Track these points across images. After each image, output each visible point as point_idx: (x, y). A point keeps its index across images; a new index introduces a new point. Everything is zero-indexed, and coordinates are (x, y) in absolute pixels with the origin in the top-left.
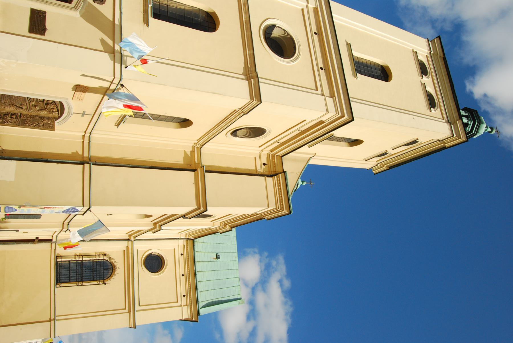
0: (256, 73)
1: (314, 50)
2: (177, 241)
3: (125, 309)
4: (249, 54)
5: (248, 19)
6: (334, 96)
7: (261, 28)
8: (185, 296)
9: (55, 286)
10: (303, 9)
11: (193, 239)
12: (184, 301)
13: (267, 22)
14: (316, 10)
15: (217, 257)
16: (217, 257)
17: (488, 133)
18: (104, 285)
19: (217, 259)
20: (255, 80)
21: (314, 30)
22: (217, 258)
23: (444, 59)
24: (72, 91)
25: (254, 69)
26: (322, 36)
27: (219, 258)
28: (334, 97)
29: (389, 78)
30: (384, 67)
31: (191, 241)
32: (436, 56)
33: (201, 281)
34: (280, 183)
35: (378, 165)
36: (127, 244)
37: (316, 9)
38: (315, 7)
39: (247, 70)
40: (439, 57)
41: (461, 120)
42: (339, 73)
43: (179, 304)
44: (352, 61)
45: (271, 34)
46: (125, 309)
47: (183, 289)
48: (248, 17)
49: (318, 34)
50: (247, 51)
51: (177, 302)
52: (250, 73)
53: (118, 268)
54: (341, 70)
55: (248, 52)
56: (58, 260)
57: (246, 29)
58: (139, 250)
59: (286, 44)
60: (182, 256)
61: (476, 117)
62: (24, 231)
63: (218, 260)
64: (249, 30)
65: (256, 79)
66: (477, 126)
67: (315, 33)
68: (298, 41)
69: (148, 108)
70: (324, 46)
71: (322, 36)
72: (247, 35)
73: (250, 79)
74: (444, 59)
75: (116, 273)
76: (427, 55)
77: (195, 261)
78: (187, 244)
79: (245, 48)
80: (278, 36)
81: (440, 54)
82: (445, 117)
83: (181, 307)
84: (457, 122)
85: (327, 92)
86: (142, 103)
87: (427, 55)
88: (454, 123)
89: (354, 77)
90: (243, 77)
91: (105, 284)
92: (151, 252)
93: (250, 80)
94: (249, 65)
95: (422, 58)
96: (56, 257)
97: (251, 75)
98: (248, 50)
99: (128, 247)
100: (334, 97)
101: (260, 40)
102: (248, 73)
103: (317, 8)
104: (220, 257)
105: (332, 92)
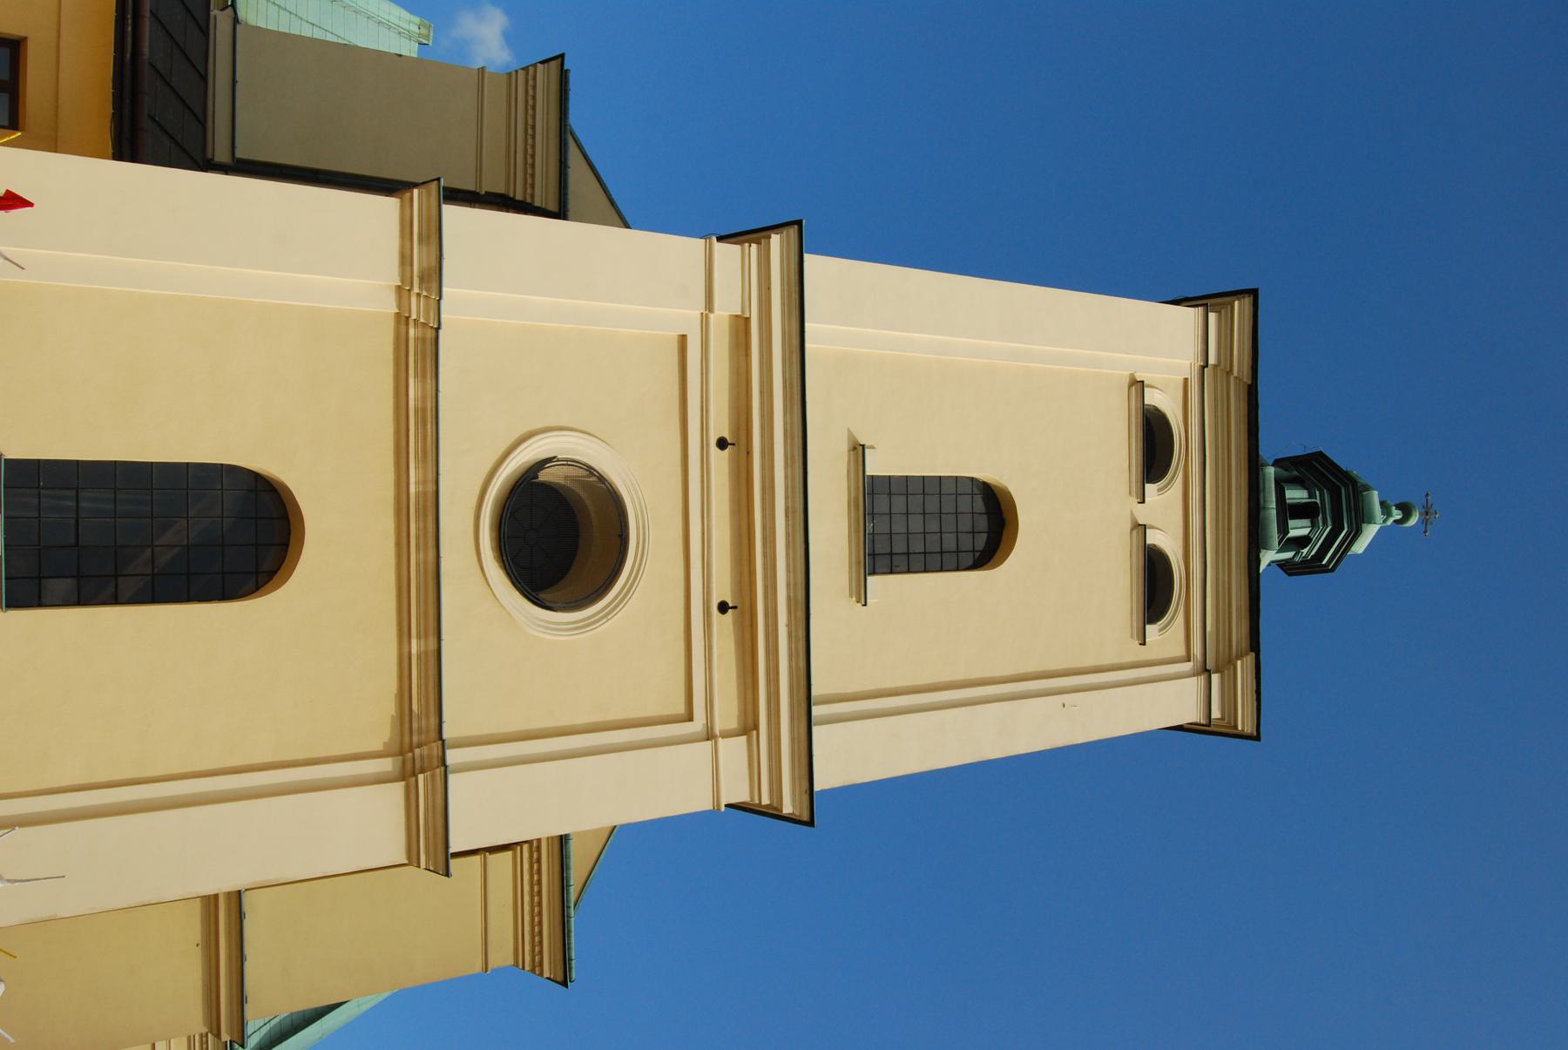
0: (440, 742)
1: (703, 534)
4: (419, 656)
5: (431, 488)
6: (756, 727)
7: (487, 498)
10: (683, 339)
13: (519, 457)
14: (740, 326)
17: (1396, 525)
20: (433, 776)
21: (723, 590)
23: (1252, 392)
25: (433, 721)
26: (749, 453)
28: (755, 732)
29: (1005, 533)
30: (993, 488)
32: (1225, 376)
34: (539, 871)
37: (742, 322)
38: (739, 313)
39: (407, 726)
40: (1235, 383)
41: (1253, 654)
42: (789, 626)
44: (857, 531)
48: (431, 476)
49: (733, 444)
50: (414, 642)
52: (415, 739)
54: (801, 614)
55: (419, 645)
57: (417, 538)
61: (1349, 511)
64: (431, 542)
65: (439, 771)
66: (1344, 543)
68: (638, 498)
70: (748, 506)
71: (748, 453)
72: (418, 564)
73: (414, 774)
74: (1252, 392)
76: (1186, 379)
79: (406, 629)
80: (562, 482)
81: (1239, 371)
82: (1197, 650)
84: (1239, 662)
85: (727, 714)
86: (8, 146)
87: (1186, 379)
88: (1225, 665)
89: (854, 599)
90: (386, 765)
93: (413, 779)
94: (415, 707)
95: (1165, 400)
97: (417, 751)
98: (419, 637)
100: (755, 732)
101: (475, 558)
102: (407, 739)
103: (747, 320)
105: (750, 707)
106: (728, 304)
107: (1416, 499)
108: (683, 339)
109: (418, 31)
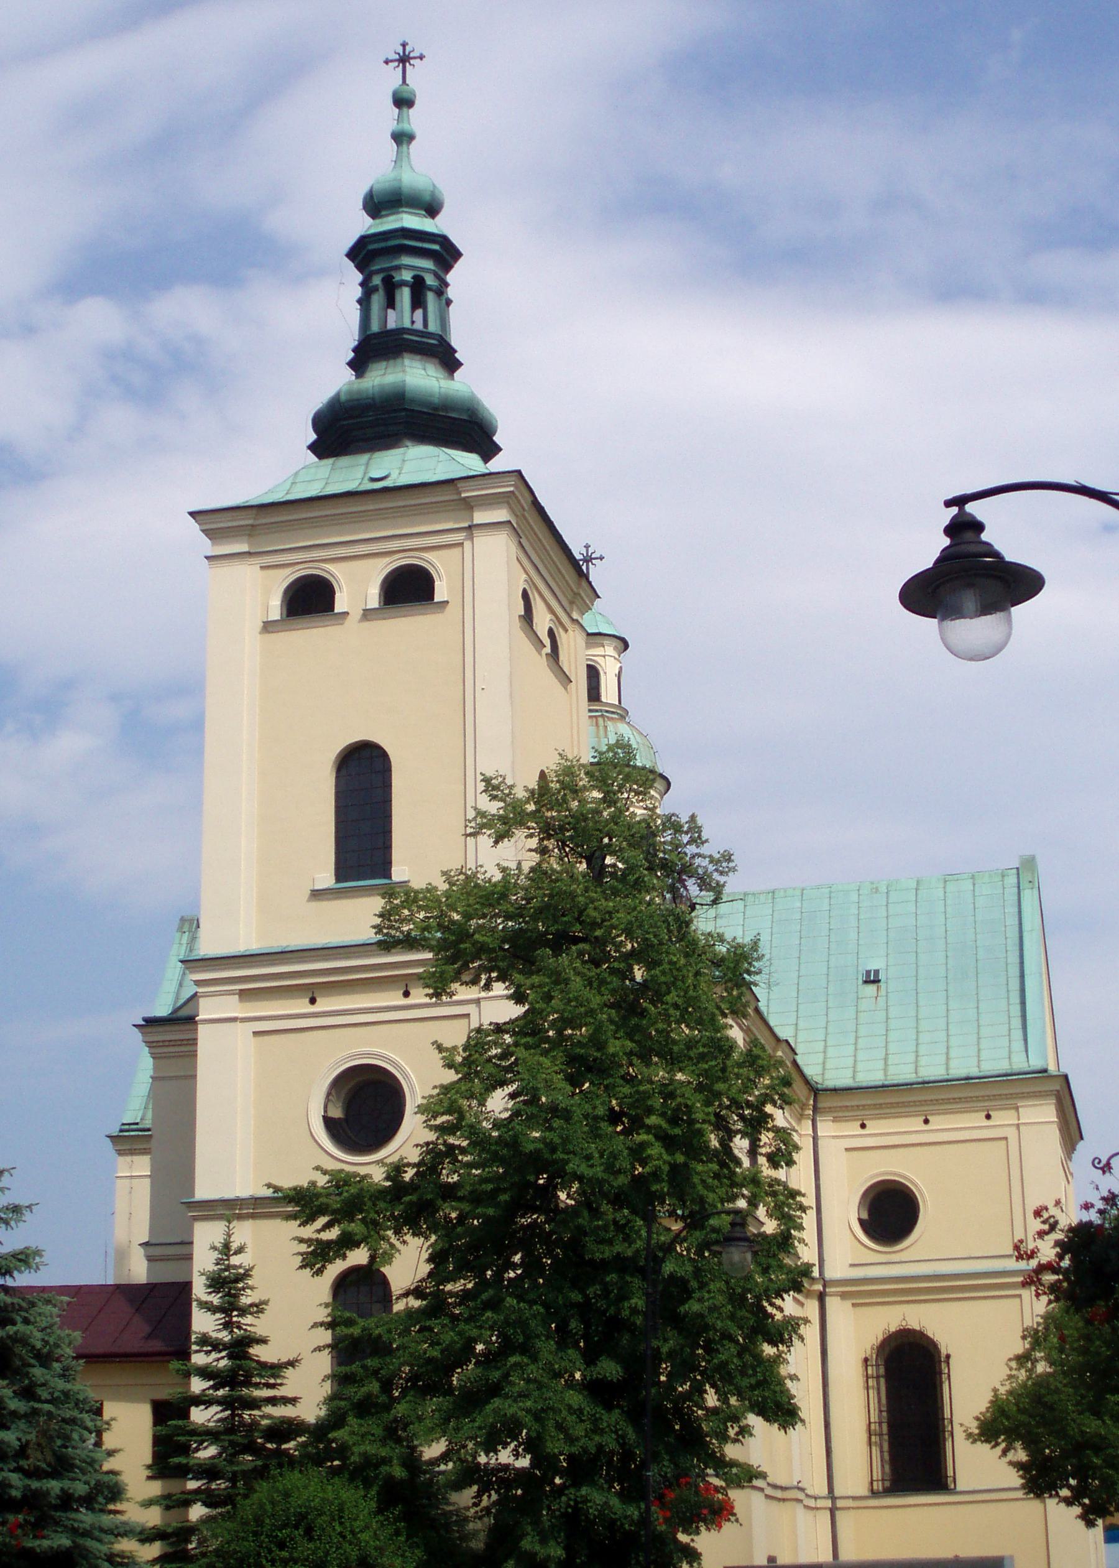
2: (820, 1142)
3: (1020, 1296)
8: (991, 1113)
9: (953, 1492)
11: (815, 1096)
12: (1001, 1118)
15: (872, 979)
16: (872, 979)
18: (951, 1361)
19: (879, 981)
22: (876, 981)
24: (149, 1478)
27: (877, 972)
31: (820, 1098)
33: (947, 1054)
35: (575, 617)
36: (833, 1298)
43: (1011, 1133)
45: (339, 1119)
46: (1020, 1296)
47: (970, 1122)
51: (1006, 1139)
53: (904, 1323)
56: (881, 1488)
58: (850, 1262)
59: (352, 1084)
60: (868, 1125)
62: (1070, 1078)
63: (881, 976)
67: (313, 1001)
69: (741, 1525)
75: (918, 1328)
77: (883, 1086)
78: (830, 1110)
83: (838, 1513)
91: (948, 1357)
92: (857, 1221)
96: (874, 1494)
99: (844, 1296)
104: (872, 967)
106: (231, 1007)
107: (392, 78)
108: (256, 1034)
109: (187, 933)
